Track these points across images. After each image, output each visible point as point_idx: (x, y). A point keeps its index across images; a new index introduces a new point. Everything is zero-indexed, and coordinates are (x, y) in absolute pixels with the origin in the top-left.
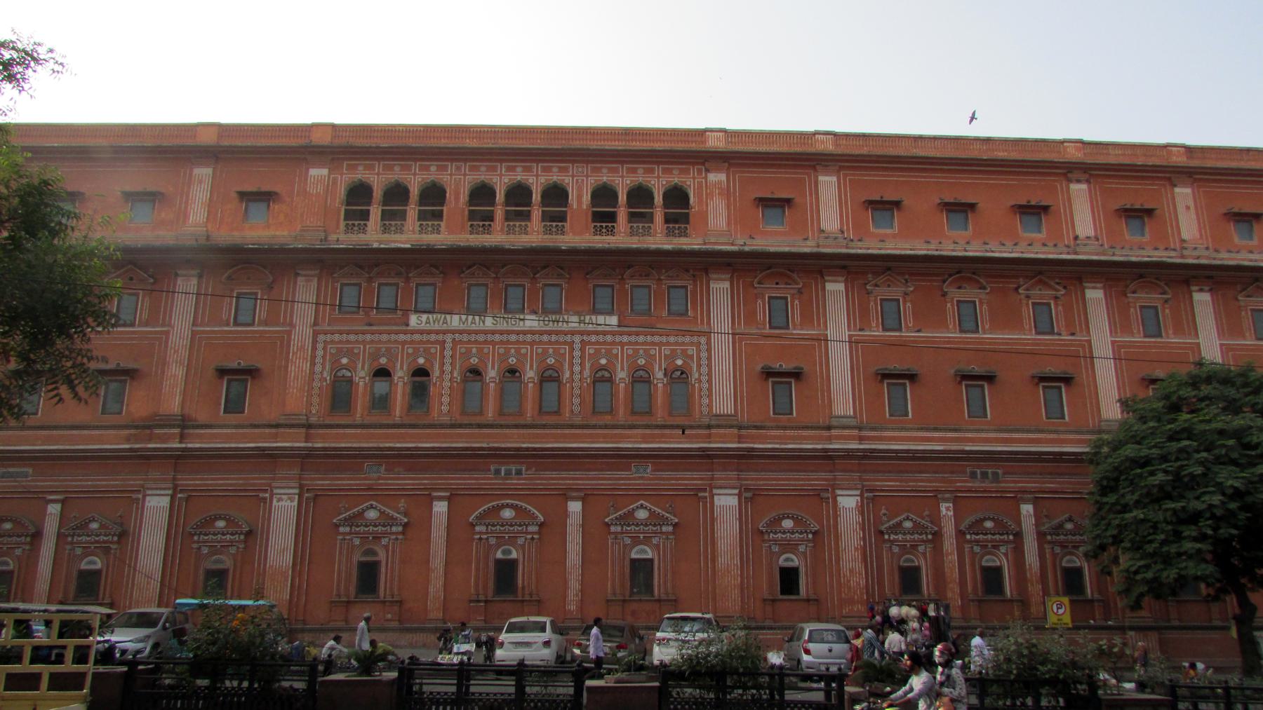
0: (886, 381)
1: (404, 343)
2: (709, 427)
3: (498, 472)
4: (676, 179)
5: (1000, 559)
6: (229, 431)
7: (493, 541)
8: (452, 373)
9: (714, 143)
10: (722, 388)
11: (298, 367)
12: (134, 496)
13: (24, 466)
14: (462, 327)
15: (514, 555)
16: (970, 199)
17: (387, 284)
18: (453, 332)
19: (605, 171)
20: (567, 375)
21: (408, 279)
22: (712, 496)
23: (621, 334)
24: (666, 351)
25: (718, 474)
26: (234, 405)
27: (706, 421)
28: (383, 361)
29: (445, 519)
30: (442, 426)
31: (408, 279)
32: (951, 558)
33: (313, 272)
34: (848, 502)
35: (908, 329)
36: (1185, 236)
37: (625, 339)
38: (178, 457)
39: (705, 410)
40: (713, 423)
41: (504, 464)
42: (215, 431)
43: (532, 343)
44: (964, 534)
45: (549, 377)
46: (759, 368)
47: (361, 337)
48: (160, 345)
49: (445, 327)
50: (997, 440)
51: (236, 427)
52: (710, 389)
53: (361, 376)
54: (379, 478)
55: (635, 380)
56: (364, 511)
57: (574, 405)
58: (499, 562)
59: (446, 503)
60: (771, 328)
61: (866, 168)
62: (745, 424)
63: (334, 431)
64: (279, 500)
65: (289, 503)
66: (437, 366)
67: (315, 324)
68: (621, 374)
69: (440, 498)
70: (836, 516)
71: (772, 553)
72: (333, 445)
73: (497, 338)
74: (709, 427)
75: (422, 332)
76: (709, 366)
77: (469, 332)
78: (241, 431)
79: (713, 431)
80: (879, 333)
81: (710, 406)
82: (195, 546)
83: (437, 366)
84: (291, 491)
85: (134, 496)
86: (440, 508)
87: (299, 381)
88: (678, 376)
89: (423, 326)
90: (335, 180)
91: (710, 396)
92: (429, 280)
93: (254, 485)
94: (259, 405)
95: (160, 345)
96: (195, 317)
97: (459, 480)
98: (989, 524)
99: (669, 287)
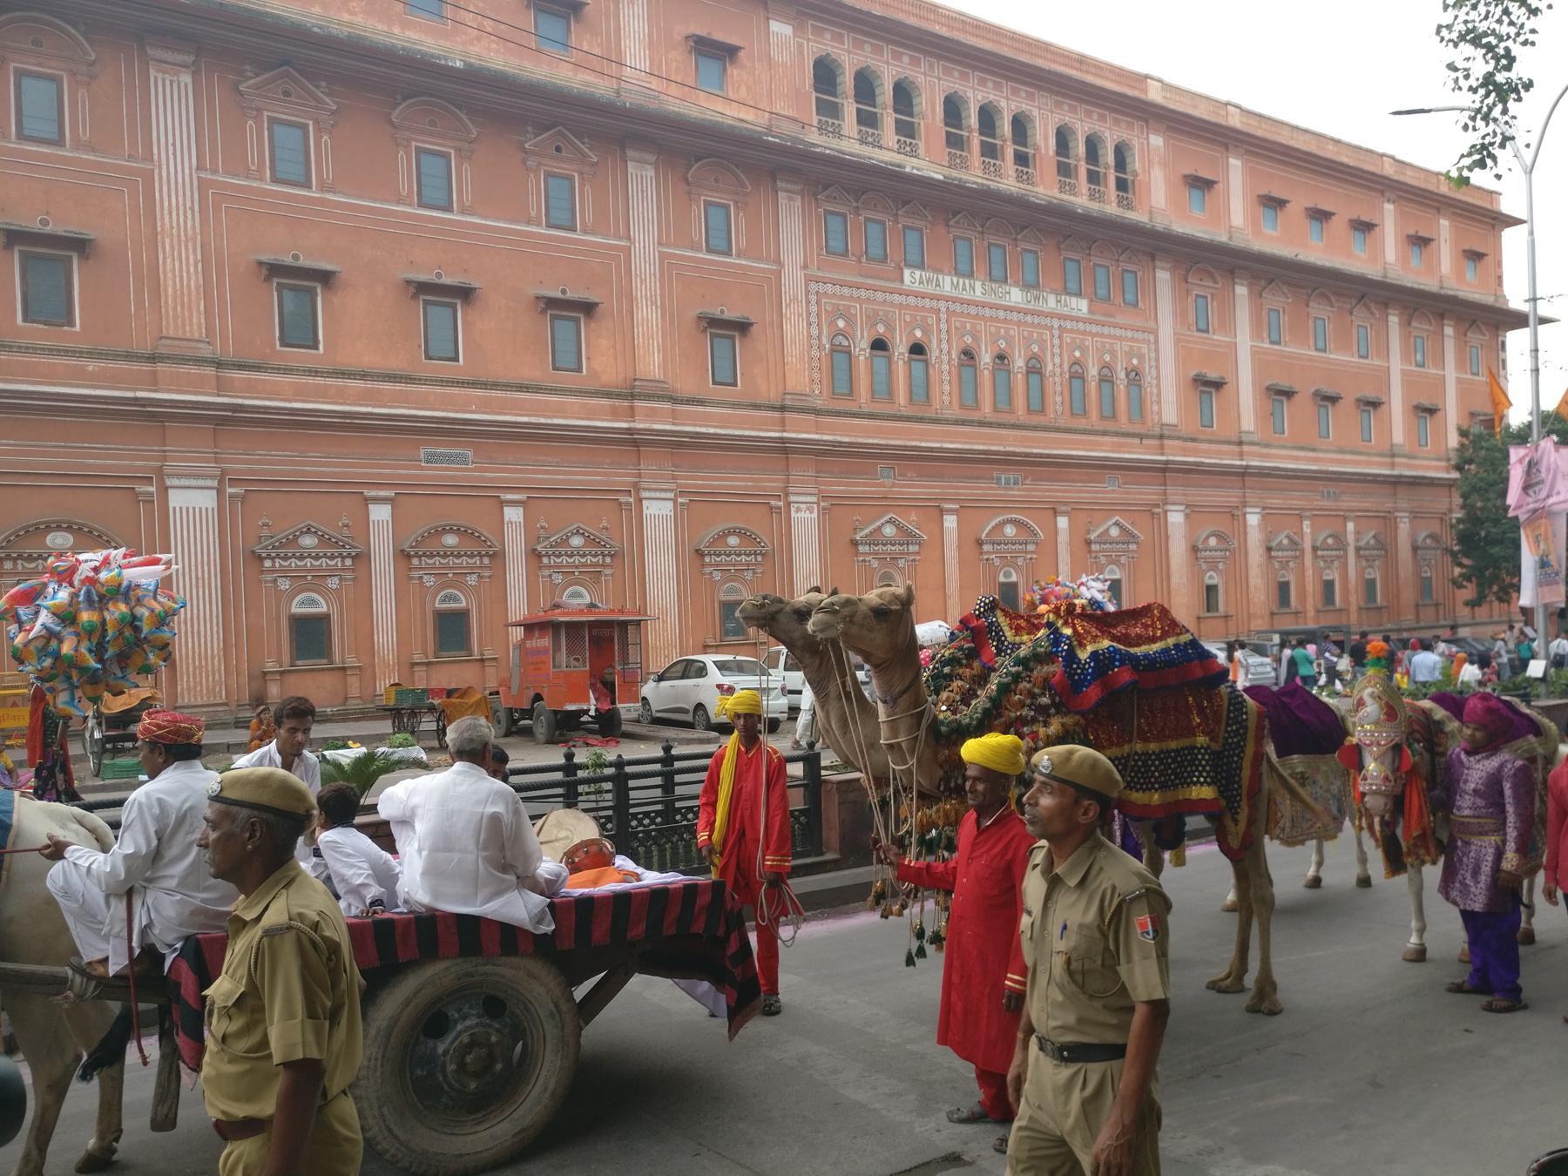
0: (275, 281)
1: (901, 306)
2: (153, 358)
3: (999, 479)
4: (1067, 119)
5: (1333, 574)
6: (725, 411)
7: (997, 562)
8: (819, 338)
9: (1154, 95)
10: (647, 336)
11: (795, 328)
12: (623, 499)
13: (458, 445)
14: (955, 293)
15: (1014, 578)
16: (733, 40)
17: (912, 228)
18: (947, 299)
19: (828, 36)
20: (1050, 367)
21: (896, 221)
22: (164, 490)
23: (1085, 321)
24: (1126, 345)
25: (1170, 490)
26: (300, 333)
27: (1157, 430)
28: (881, 329)
29: (955, 538)
30: (947, 422)
31: (896, 221)
32: (1309, 573)
33: (180, 58)
34: (658, 510)
35: (78, 145)
36: (1154, 203)
37: (1094, 329)
38: (224, 421)
39: (1156, 418)
40: (788, 403)
41: (1005, 471)
42: (708, 409)
43: (1019, 323)
44: (261, 559)
45: (1035, 369)
46: (1193, 373)
47: (855, 293)
48: (618, 266)
49: (938, 291)
50: (1331, 461)
51: (735, 405)
52: (1159, 395)
53: (861, 347)
54: (894, 485)
55: (1031, 371)
56: (880, 528)
57: (945, 396)
58: (1002, 585)
59: (389, 507)
60: (21, 136)
61: (1339, 179)
62: (230, 354)
63: (184, 369)
64: (798, 510)
65: (808, 514)
66: (935, 342)
67: (805, 267)
68: (1093, 371)
69: (951, 511)
70: (1245, 533)
71: (554, 586)
72: (860, 440)
73: (988, 312)
74: (153, 358)
75: (917, 295)
76: (1158, 368)
77: (962, 302)
78: (738, 412)
79: (160, 367)
80: (1267, 346)
81: (1159, 413)
82: (269, 577)
83: (935, 342)
84: (809, 499)
85: (623, 499)
86: (950, 522)
87: (795, 346)
88: (1135, 376)
89: (917, 287)
90: (800, 46)
91: (1159, 402)
92: (918, 223)
93: (764, 488)
94: (601, 358)
95: (618, 266)
96: (660, 236)
97: (969, 489)
98: (577, 541)
99: (867, 219)
